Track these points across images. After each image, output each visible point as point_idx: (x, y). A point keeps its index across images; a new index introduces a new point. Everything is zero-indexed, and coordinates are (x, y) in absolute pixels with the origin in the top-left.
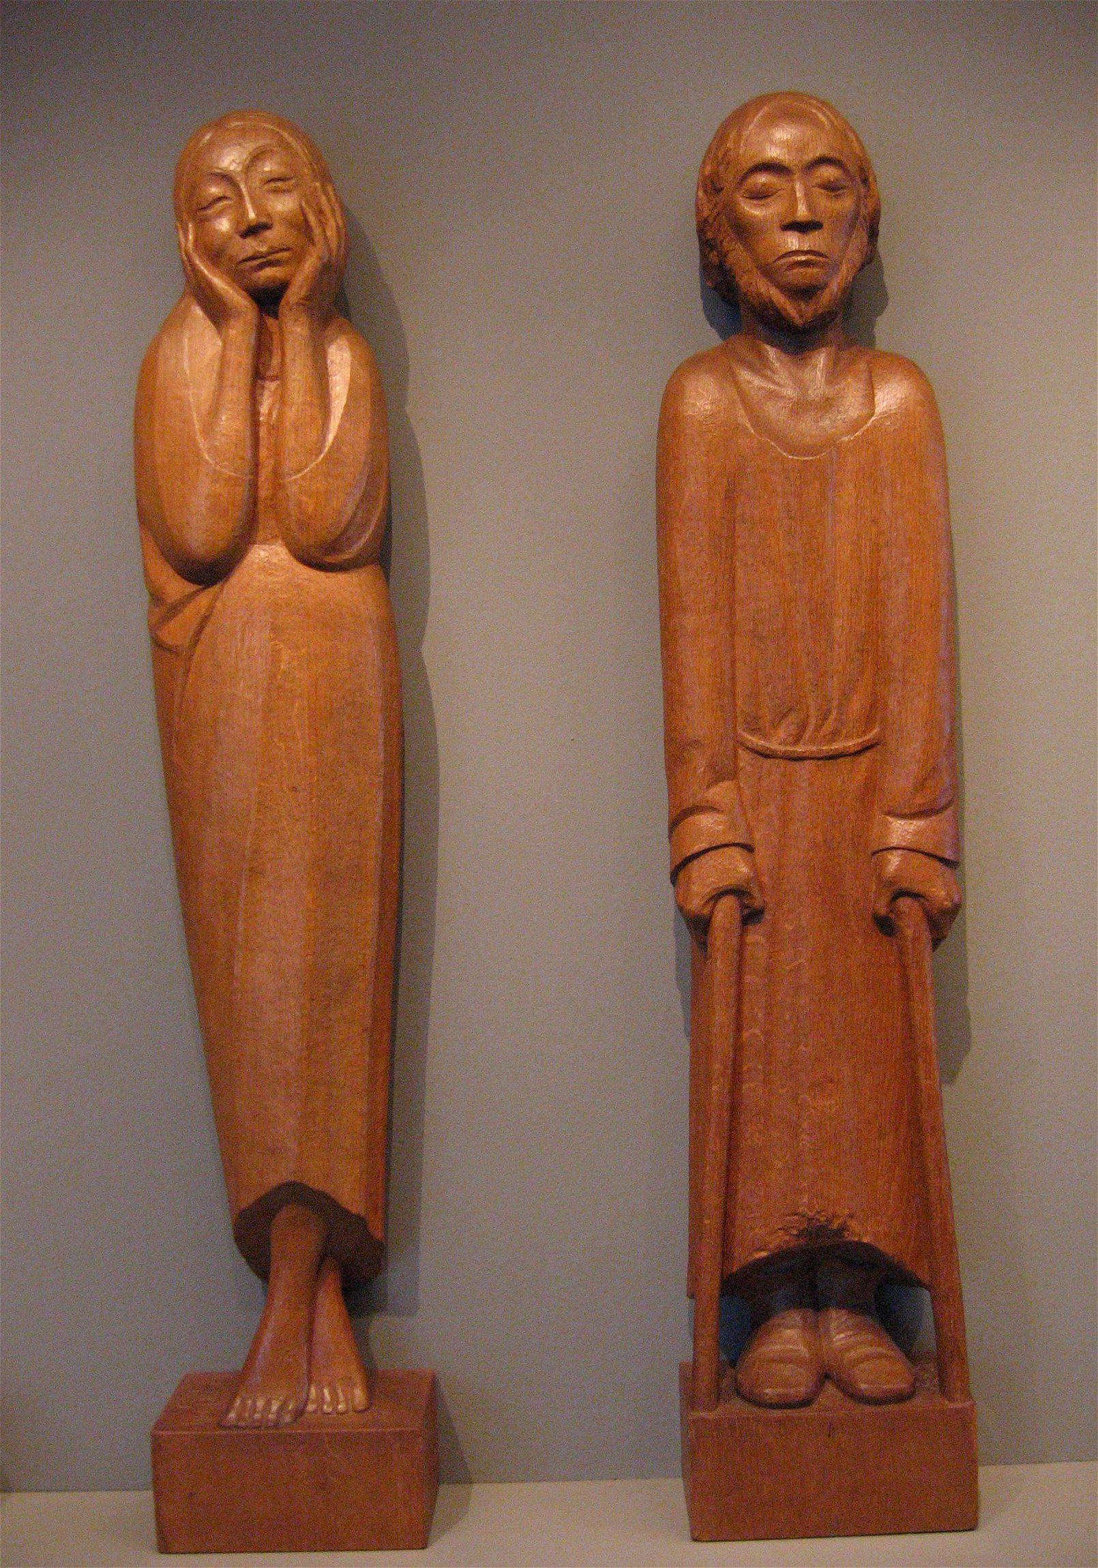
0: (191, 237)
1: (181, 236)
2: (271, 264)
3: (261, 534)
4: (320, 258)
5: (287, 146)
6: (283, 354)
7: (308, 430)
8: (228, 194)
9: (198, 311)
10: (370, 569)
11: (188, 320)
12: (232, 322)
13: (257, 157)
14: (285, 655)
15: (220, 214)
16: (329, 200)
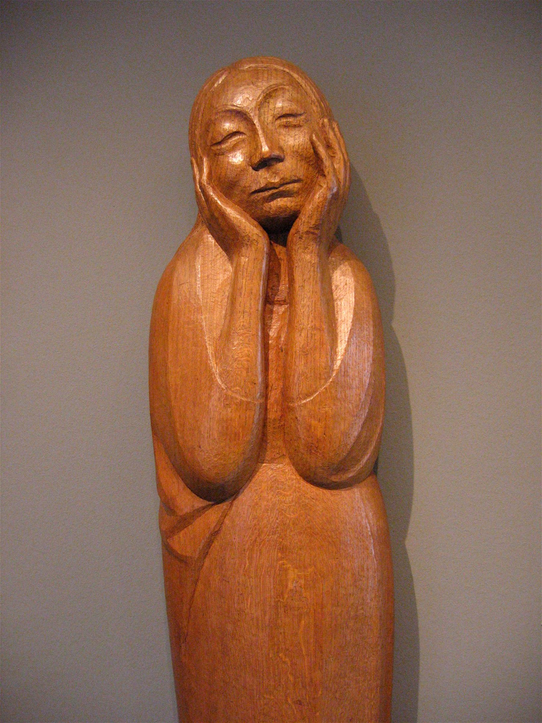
0: (205, 170)
1: (196, 169)
2: (282, 195)
3: (269, 454)
4: (329, 189)
5: (297, 86)
6: (292, 281)
7: (317, 355)
8: (242, 130)
9: (211, 240)
10: (369, 480)
11: (201, 248)
12: (244, 250)
13: (269, 95)
14: (292, 574)
15: (234, 148)
16: (335, 135)
